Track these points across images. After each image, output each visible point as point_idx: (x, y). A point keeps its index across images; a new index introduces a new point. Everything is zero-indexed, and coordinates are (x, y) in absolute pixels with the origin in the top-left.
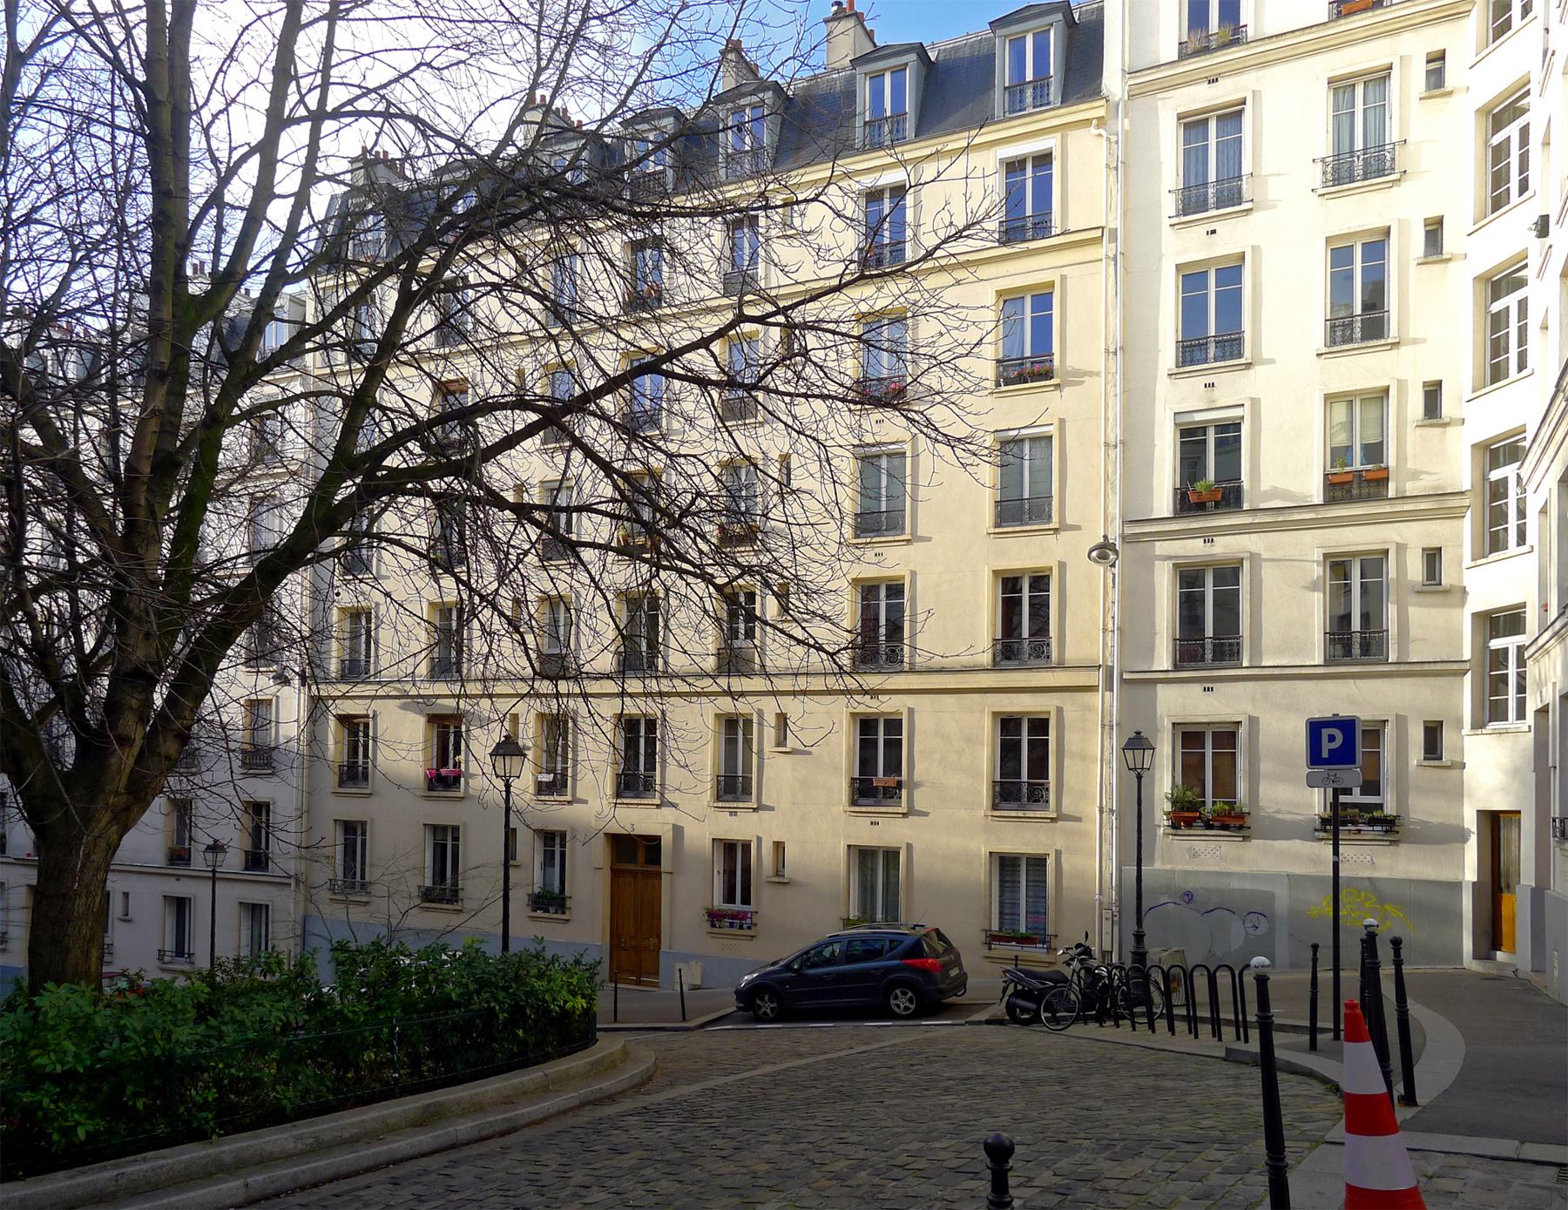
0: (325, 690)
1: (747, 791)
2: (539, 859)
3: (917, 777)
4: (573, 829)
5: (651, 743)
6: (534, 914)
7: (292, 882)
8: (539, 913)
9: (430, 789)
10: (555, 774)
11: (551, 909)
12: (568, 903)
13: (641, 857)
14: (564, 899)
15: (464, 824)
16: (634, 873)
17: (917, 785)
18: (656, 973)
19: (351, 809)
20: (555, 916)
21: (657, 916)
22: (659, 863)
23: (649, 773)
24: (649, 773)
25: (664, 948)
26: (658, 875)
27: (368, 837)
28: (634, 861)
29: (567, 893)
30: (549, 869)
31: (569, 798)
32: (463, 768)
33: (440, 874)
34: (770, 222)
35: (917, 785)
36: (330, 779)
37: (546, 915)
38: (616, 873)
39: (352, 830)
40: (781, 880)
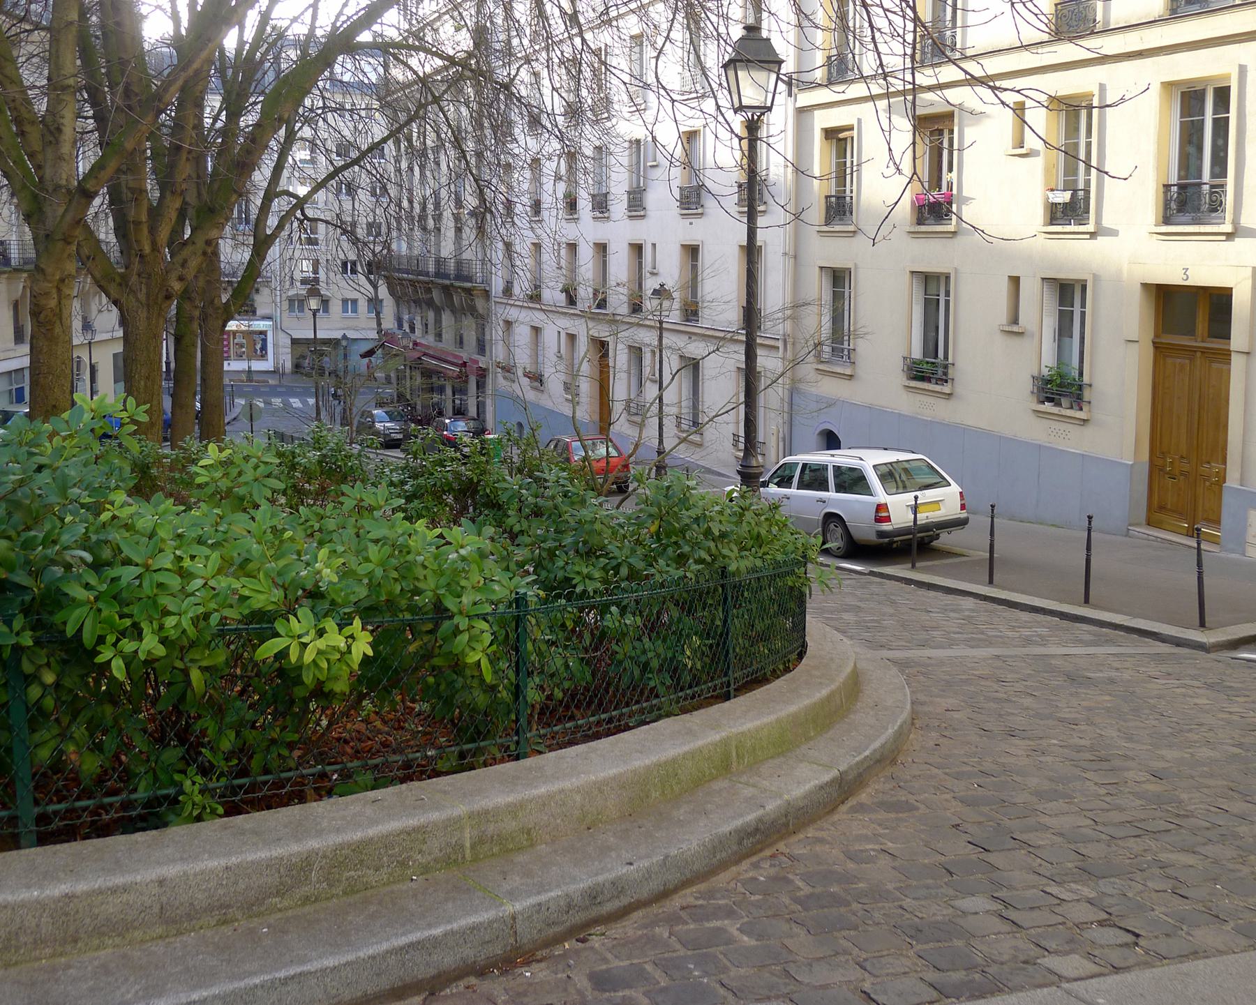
0: (805, 99)
1: (1216, 206)
2: (1050, 324)
3: (965, 193)
4: (1096, 277)
5: (1221, 127)
6: (1042, 407)
7: (780, 344)
8: (1048, 407)
9: (920, 222)
10: (1075, 191)
11: (1065, 402)
12: (1087, 394)
13: (1202, 325)
14: (1080, 387)
15: (956, 270)
16: (1190, 352)
17: (967, 200)
18: (1216, 522)
19: (834, 252)
20: (1069, 413)
21: (1221, 423)
22: (1227, 336)
23: (1218, 181)
24: (1218, 181)
25: (1232, 481)
26: (1226, 355)
27: (951, 298)
28: (1191, 332)
29: (1086, 379)
30: (1067, 340)
31: (1228, 228)
32: (955, 191)
33: (931, 346)
34: (344, 70)
35: (967, 200)
36: (816, 214)
37: (1056, 410)
38: (1159, 348)
39: (839, 278)
40: (1015, 329)
